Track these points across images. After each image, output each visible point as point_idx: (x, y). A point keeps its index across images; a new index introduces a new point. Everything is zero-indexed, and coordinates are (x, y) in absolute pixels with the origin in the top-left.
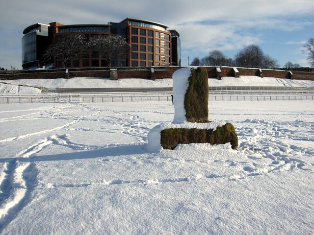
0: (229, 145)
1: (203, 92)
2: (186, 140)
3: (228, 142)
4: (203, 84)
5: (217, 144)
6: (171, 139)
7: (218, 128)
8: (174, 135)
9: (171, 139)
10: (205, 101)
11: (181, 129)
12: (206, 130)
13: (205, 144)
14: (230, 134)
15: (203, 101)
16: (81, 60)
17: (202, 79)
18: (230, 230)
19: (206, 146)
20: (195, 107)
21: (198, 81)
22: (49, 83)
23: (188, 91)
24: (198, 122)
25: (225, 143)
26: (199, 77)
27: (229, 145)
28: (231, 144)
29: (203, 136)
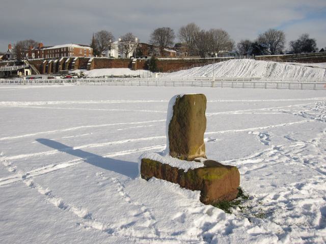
0: (198, 194)
1: (184, 125)
2: (160, 174)
3: (197, 189)
4: (185, 115)
5: (186, 189)
6: (151, 169)
7: (190, 170)
8: (151, 167)
9: (151, 169)
10: (186, 136)
11: (156, 161)
12: (177, 169)
13: (174, 184)
14: (201, 181)
15: (184, 135)
16: (175, 52)
17: (185, 109)
18: (114, 210)
19: (173, 188)
20: (176, 141)
21: (180, 112)
22: (290, 63)
23: (171, 121)
24: (179, 158)
25: (193, 190)
26: (181, 107)
27: (198, 194)
28: (201, 194)
29: (174, 175)
